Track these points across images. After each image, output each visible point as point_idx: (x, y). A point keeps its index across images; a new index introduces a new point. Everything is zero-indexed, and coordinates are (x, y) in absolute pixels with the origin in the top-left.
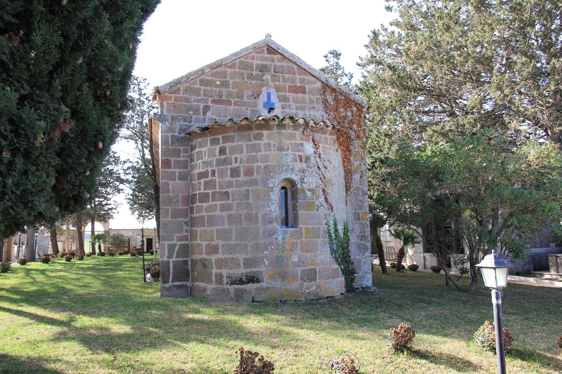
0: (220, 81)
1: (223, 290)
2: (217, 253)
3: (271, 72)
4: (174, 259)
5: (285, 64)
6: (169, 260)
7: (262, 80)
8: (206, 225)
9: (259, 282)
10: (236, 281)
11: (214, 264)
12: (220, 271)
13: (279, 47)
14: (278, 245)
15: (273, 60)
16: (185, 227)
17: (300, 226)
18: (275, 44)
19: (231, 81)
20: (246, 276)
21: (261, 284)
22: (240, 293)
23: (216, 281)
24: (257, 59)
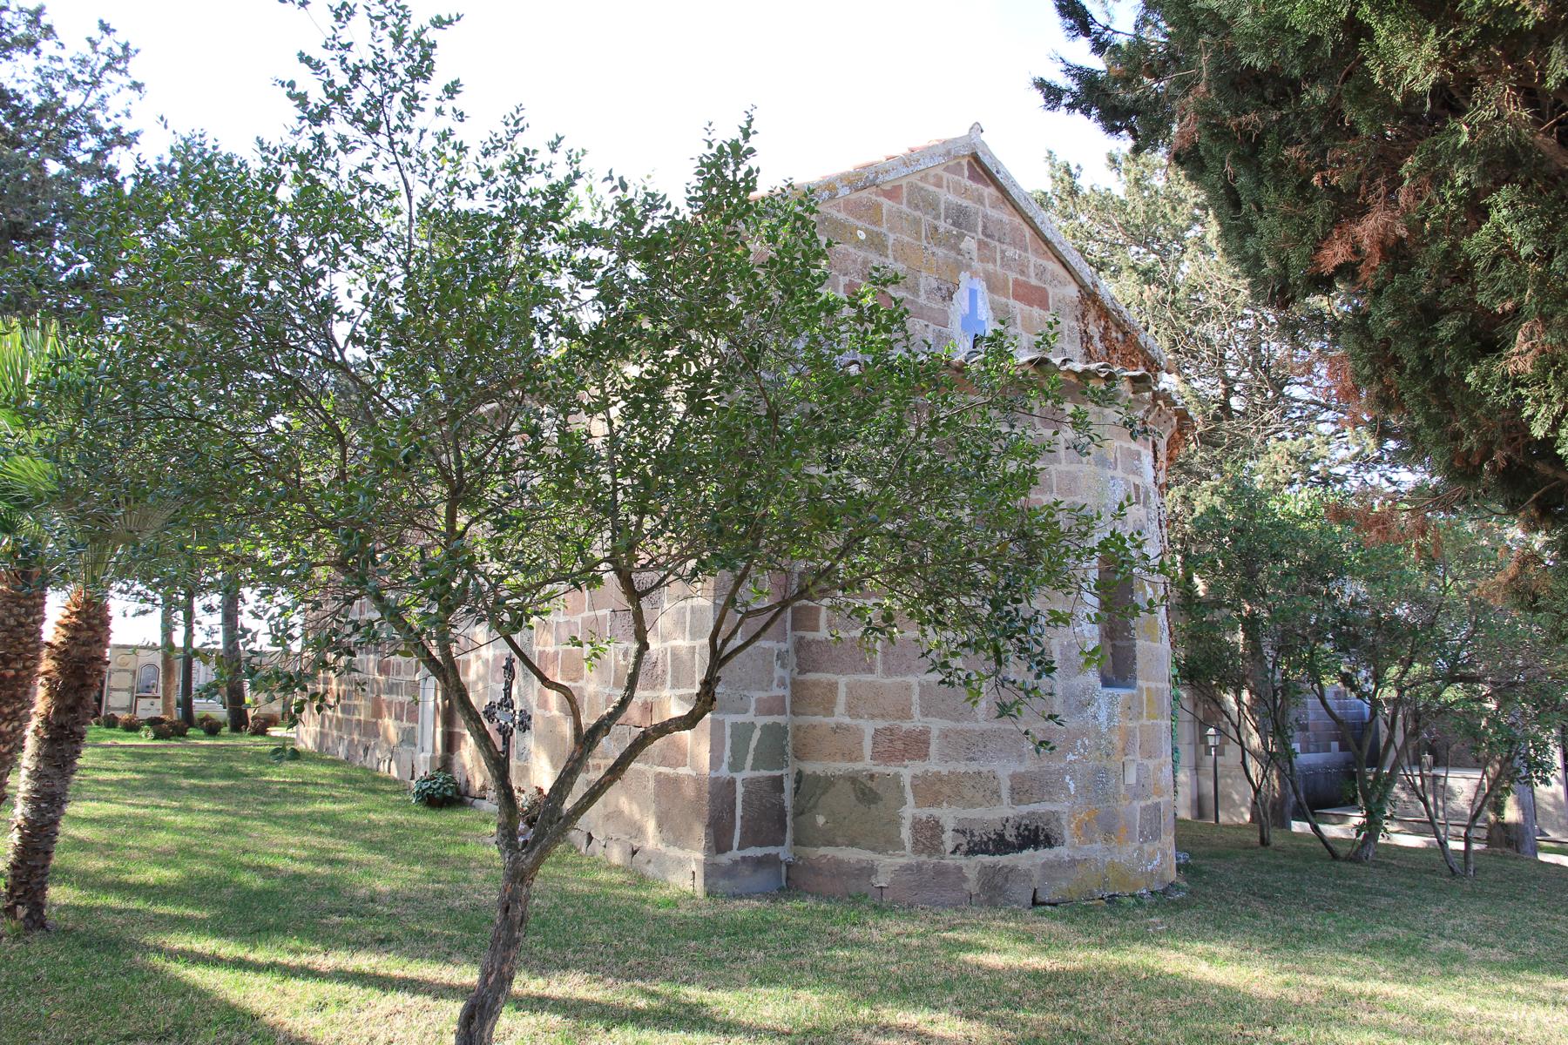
0: (866, 231)
1: (941, 872)
2: (924, 756)
3: (976, 232)
4: (747, 773)
5: (1006, 218)
6: (735, 775)
7: (959, 252)
8: (879, 667)
9: (1051, 846)
10: (986, 843)
11: (908, 788)
12: (935, 811)
13: (1001, 170)
14: (1099, 735)
15: (980, 200)
16: (778, 672)
17: (1140, 682)
18: (992, 156)
19: (891, 237)
20: (1018, 828)
21: (1056, 850)
22: (999, 880)
23: (916, 842)
24: (948, 187)
